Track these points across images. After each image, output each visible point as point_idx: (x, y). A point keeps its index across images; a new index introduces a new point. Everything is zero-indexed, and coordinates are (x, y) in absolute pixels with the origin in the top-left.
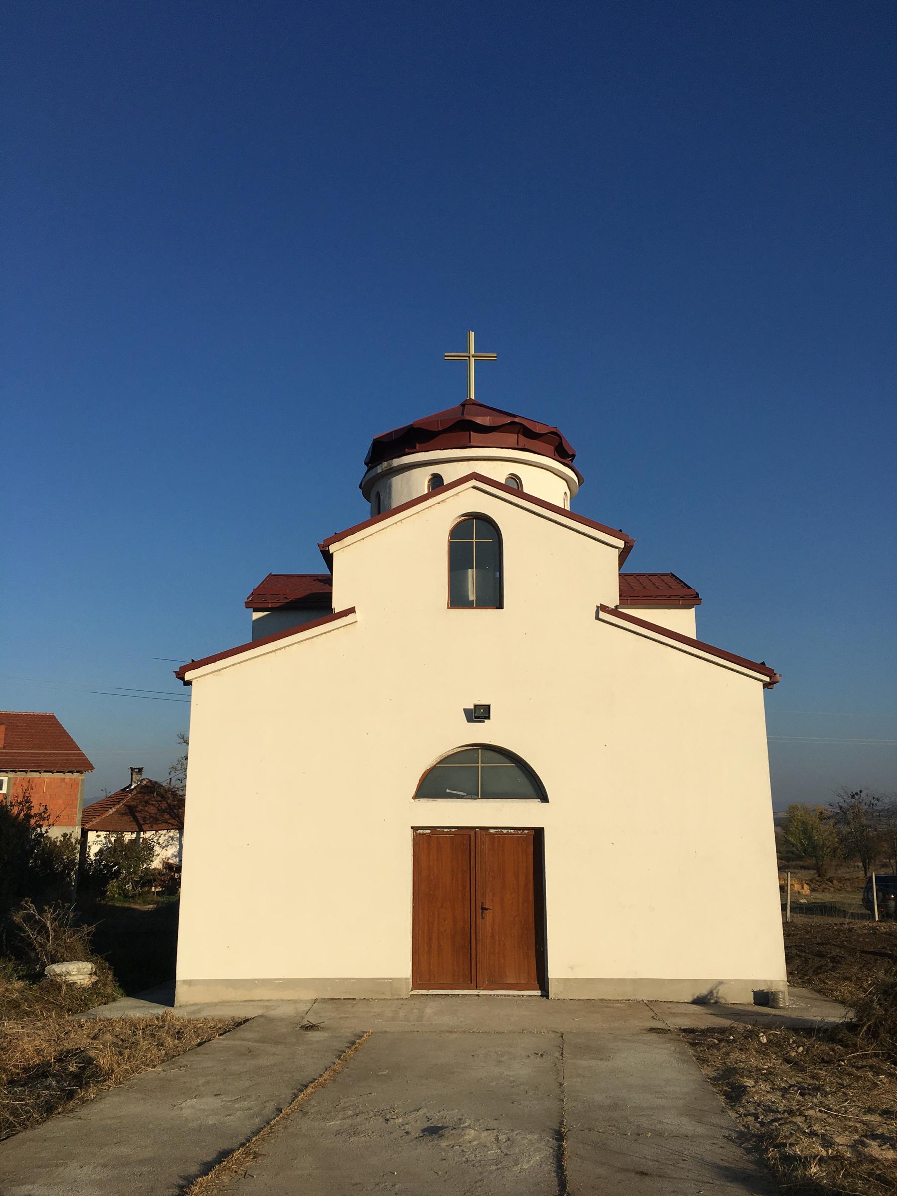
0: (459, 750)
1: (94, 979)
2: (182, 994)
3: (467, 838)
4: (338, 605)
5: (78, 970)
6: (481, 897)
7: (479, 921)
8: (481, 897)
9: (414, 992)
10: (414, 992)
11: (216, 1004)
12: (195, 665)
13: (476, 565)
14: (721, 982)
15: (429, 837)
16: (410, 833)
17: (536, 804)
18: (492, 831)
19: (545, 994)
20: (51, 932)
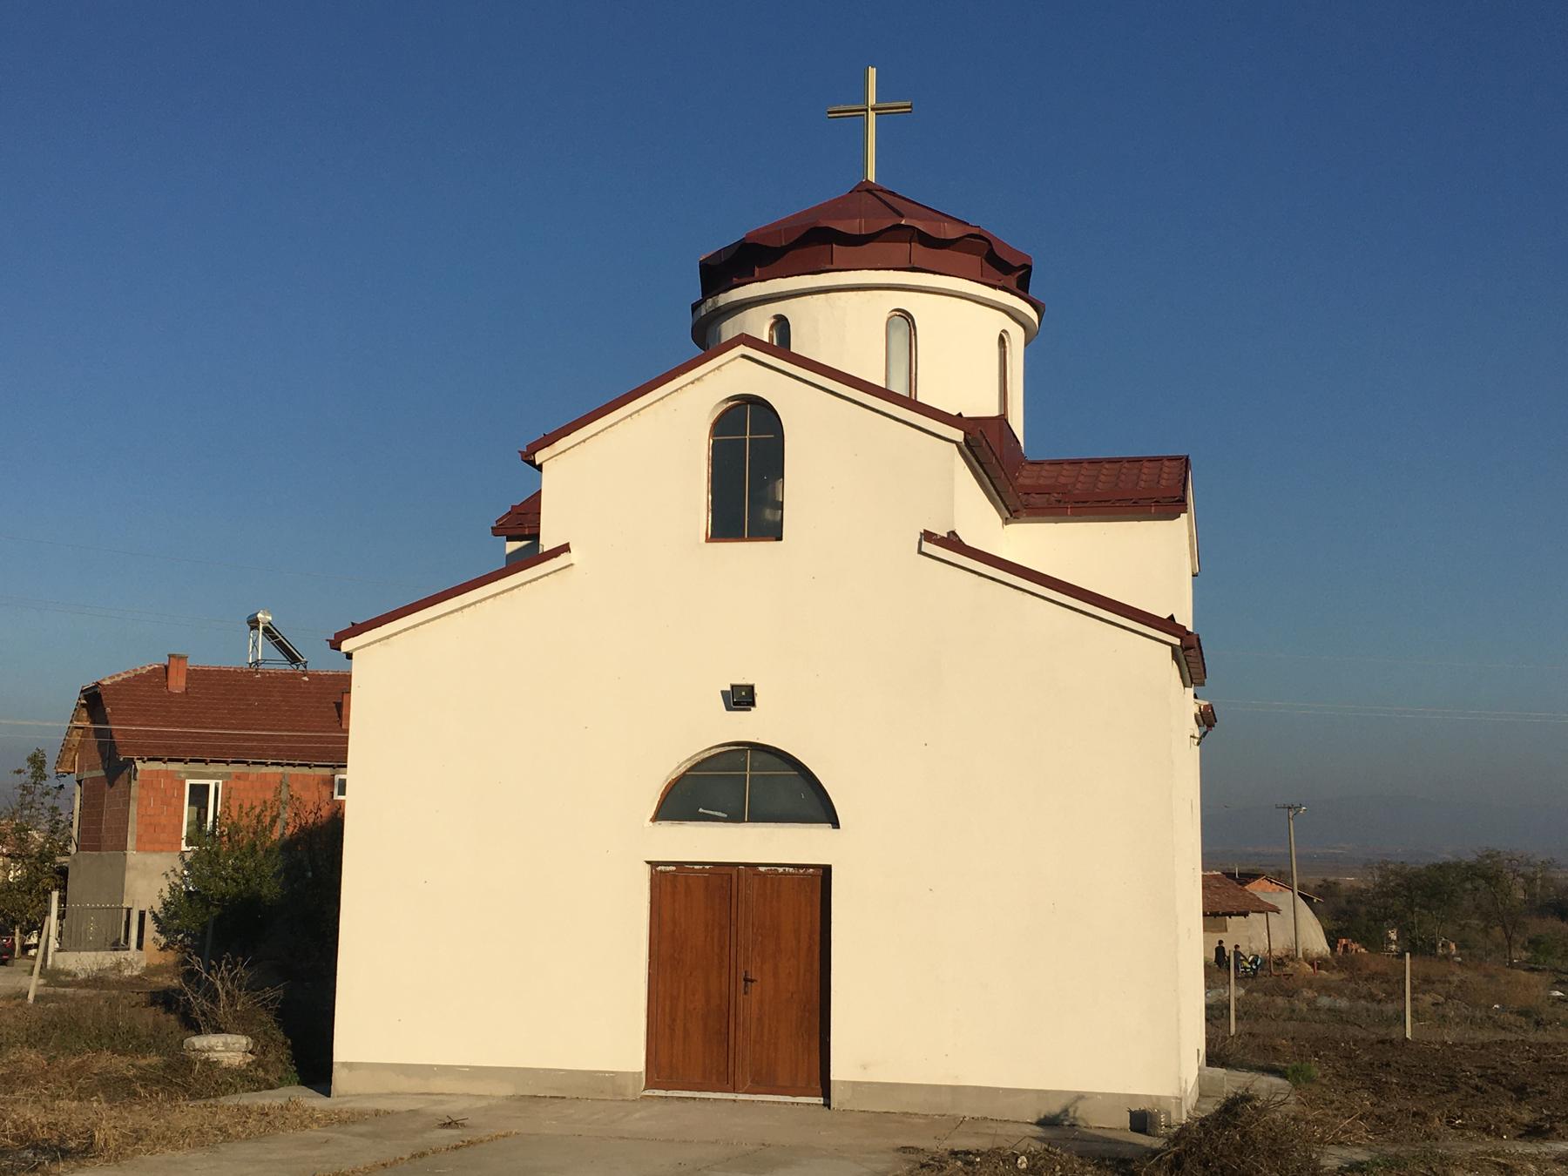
0: (707, 755)
1: (251, 1058)
2: (340, 1078)
3: (726, 879)
4: (547, 542)
5: (225, 1044)
6: (741, 964)
7: (741, 997)
8: (741, 964)
9: (647, 1093)
10: (647, 1093)
11: (380, 1095)
12: (356, 630)
13: (746, 481)
14: (1080, 1097)
15: (673, 875)
16: (645, 873)
17: (822, 831)
18: (762, 869)
19: (827, 1105)
20: (223, 995)
